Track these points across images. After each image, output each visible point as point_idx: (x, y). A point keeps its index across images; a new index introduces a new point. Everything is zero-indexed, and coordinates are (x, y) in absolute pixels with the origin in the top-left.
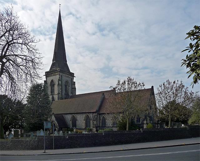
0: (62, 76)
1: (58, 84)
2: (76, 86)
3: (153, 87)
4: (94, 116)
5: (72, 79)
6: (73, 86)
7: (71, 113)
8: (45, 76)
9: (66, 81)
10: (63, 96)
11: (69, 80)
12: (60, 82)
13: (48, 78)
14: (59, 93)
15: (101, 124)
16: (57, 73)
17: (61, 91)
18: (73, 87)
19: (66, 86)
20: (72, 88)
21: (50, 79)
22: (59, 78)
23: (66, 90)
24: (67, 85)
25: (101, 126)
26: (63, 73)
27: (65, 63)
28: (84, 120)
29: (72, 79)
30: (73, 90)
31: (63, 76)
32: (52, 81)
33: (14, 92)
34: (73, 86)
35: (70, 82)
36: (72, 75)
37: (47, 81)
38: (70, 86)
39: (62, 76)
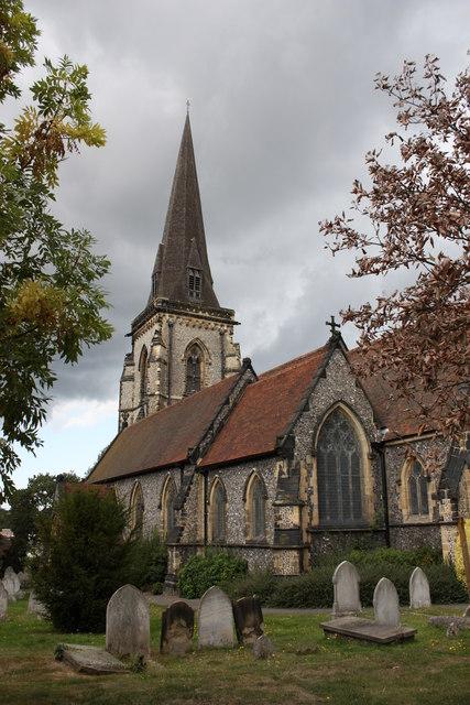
0: (171, 326)
5: (222, 334)
29: (222, 334)
31: (177, 327)
38: (216, 361)
39: (171, 326)
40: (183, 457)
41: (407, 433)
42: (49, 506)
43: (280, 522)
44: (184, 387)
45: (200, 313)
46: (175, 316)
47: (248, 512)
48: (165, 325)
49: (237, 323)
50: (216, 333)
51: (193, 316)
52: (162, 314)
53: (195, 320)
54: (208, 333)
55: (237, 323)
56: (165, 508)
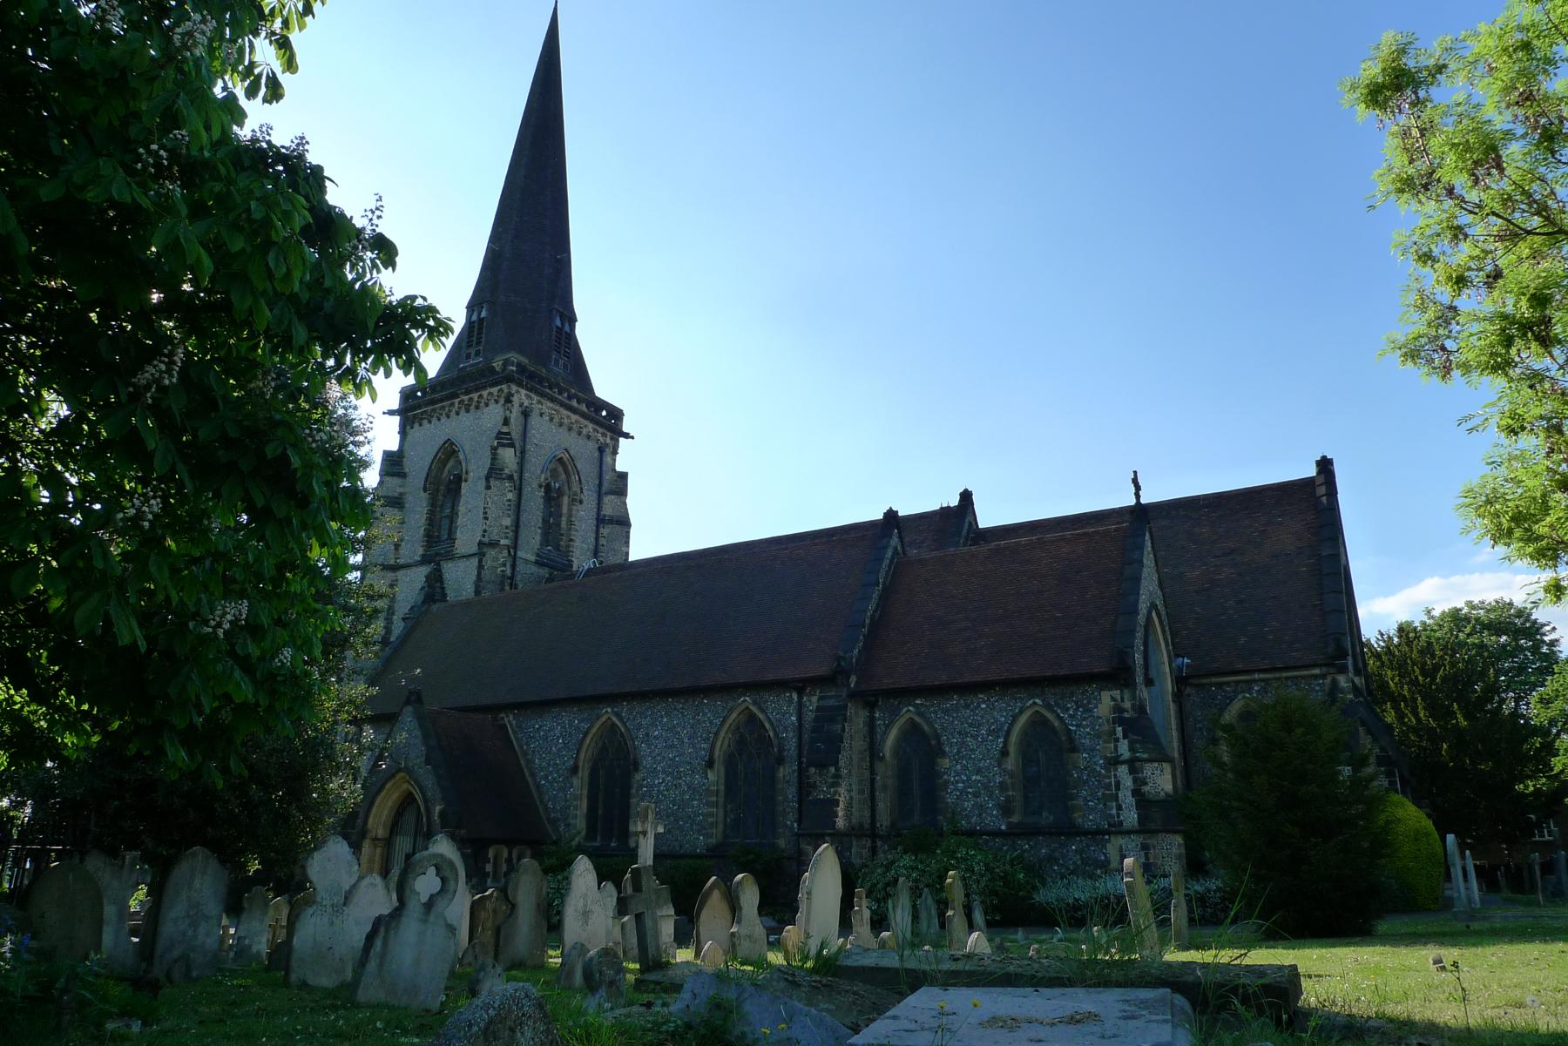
0: (526, 414)
1: (494, 472)
2: (635, 503)
3: (1325, 465)
4: (809, 716)
5: (601, 450)
6: (607, 499)
7: (968, 678)
8: (397, 419)
9: (560, 460)
10: (520, 567)
11: (583, 451)
12: (508, 456)
13: (416, 433)
14: (494, 544)
15: (882, 806)
16: (495, 390)
17: (507, 522)
18: (608, 510)
19: (552, 497)
20: (601, 520)
21: (433, 433)
22: (506, 422)
23: (552, 530)
24: (560, 492)
25: (884, 820)
26: (542, 395)
27: (560, 330)
28: (710, 764)
29: (601, 450)
30: (605, 531)
31: (534, 420)
32: (449, 451)
33: (1256, 973)
34: (609, 500)
35: (586, 467)
36: (609, 422)
37: (408, 453)
38: (589, 498)
39: (526, 414)
40: (823, 670)
41: (1240, 666)
42: (1396, 733)
43: (1146, 789)
44: (538, 538)
45: (574, 403)
46: (535, 398)
47: (1012, 775)
48: (516, 410)
49: (627, 436)
50: (592, 445)
51: (563, 405)
52: (514, 388)
53: (565, 412)
54: (582, 441)
55: (627, 436)
56: (719, 767)
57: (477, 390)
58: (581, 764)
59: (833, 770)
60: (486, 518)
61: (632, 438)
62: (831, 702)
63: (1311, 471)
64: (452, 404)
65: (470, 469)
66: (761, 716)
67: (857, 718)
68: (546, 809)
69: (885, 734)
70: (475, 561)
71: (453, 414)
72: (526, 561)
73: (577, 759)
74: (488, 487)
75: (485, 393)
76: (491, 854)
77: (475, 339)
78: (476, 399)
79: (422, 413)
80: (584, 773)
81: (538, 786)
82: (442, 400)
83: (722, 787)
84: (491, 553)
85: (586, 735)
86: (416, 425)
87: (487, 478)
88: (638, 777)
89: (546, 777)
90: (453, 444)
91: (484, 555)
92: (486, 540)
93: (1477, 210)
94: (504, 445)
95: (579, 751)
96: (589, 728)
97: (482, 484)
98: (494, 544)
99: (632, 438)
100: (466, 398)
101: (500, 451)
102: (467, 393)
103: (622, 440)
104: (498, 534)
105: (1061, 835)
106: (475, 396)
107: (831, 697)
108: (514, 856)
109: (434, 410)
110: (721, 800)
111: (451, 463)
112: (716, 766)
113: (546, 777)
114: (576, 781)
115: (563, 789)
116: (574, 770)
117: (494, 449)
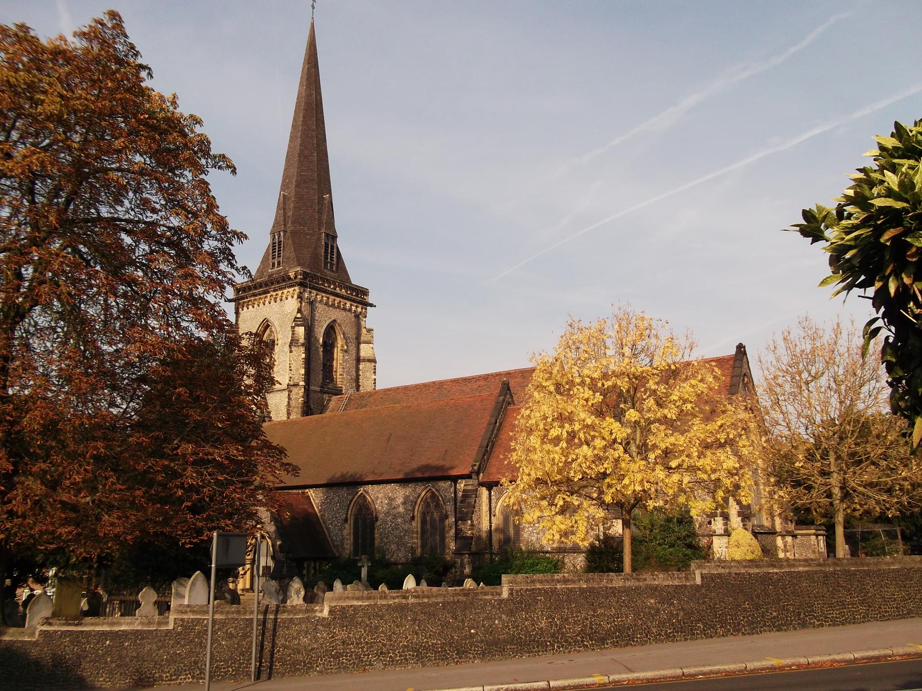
5: (357, 316)
14: (296, 385)
16: (291, 290)
29: (357, 316)
49: (371, 305)
55: (371, 305)
57: (281, 289)
58: (349, 516)
59: (469, 522)
60: (291, 370)
61: (375, 306)
62: (470, 488)
63: (733, 351)
64: (266, 297)
65: (279, 337)
66: (437, 493)
67: (484, 492)
68: (332, 540)
69: (497, 503)
70: (286, 393)
71: (267, 303)
72: (316, 391)
73: (347, 514)
74: (291, 352)
75: (285, 291)
76: (305, 566)
77: (277, 253)
78: (280, 295)
79: (249, 301)
80: (351, 521)
81: (328, 529)
82: (260, 294)
83: (419, 530)
84: (295, 390)
85: (351, 502)
86: (245, 308)
87: (290, 346)
88: (378, 523)
89: (331, 524)
90: (268, 321)
91: (291, 391)
92: (292, 383)
93: (627, 351)
94: (299, 325)
95: (348, 510)
96: (353, 498)
97: (287, 349)
98: (296, 385)
99: (375, 306)
100: (274, 294)
101: (296, 328)
102: (274, 291)
103: (368, 308)
104: (298, 379)
105: (574, 553)
106: (280, 293)
107: (469, 485)
108: (317, 565)
109: (255, 300)
110: (419, 536)
111: (268, 332)
112: (416, 519)
113: (331, 524)
114: (347, 526)
115: (341, 530)
116: (346, 520)
117: (293, 328)
